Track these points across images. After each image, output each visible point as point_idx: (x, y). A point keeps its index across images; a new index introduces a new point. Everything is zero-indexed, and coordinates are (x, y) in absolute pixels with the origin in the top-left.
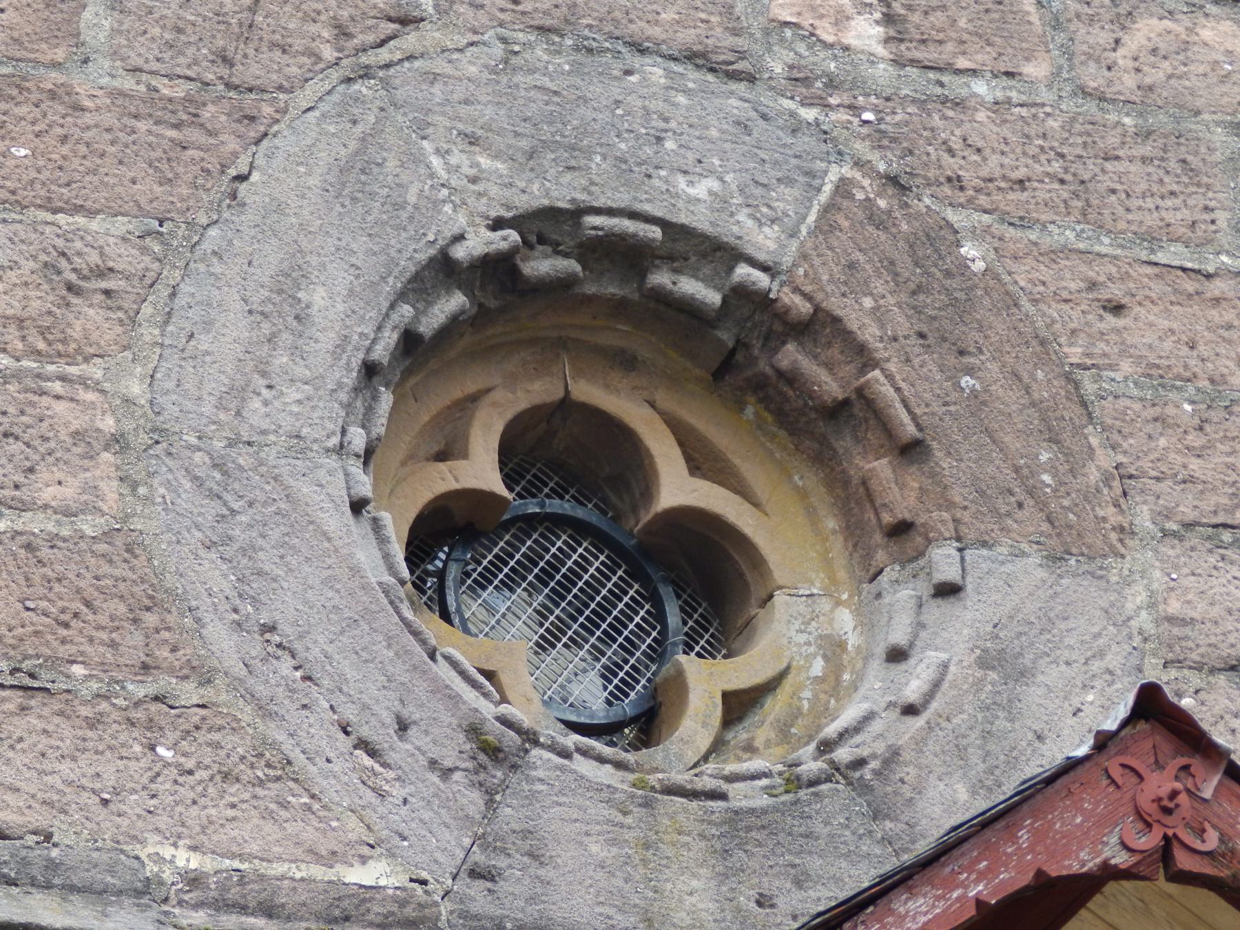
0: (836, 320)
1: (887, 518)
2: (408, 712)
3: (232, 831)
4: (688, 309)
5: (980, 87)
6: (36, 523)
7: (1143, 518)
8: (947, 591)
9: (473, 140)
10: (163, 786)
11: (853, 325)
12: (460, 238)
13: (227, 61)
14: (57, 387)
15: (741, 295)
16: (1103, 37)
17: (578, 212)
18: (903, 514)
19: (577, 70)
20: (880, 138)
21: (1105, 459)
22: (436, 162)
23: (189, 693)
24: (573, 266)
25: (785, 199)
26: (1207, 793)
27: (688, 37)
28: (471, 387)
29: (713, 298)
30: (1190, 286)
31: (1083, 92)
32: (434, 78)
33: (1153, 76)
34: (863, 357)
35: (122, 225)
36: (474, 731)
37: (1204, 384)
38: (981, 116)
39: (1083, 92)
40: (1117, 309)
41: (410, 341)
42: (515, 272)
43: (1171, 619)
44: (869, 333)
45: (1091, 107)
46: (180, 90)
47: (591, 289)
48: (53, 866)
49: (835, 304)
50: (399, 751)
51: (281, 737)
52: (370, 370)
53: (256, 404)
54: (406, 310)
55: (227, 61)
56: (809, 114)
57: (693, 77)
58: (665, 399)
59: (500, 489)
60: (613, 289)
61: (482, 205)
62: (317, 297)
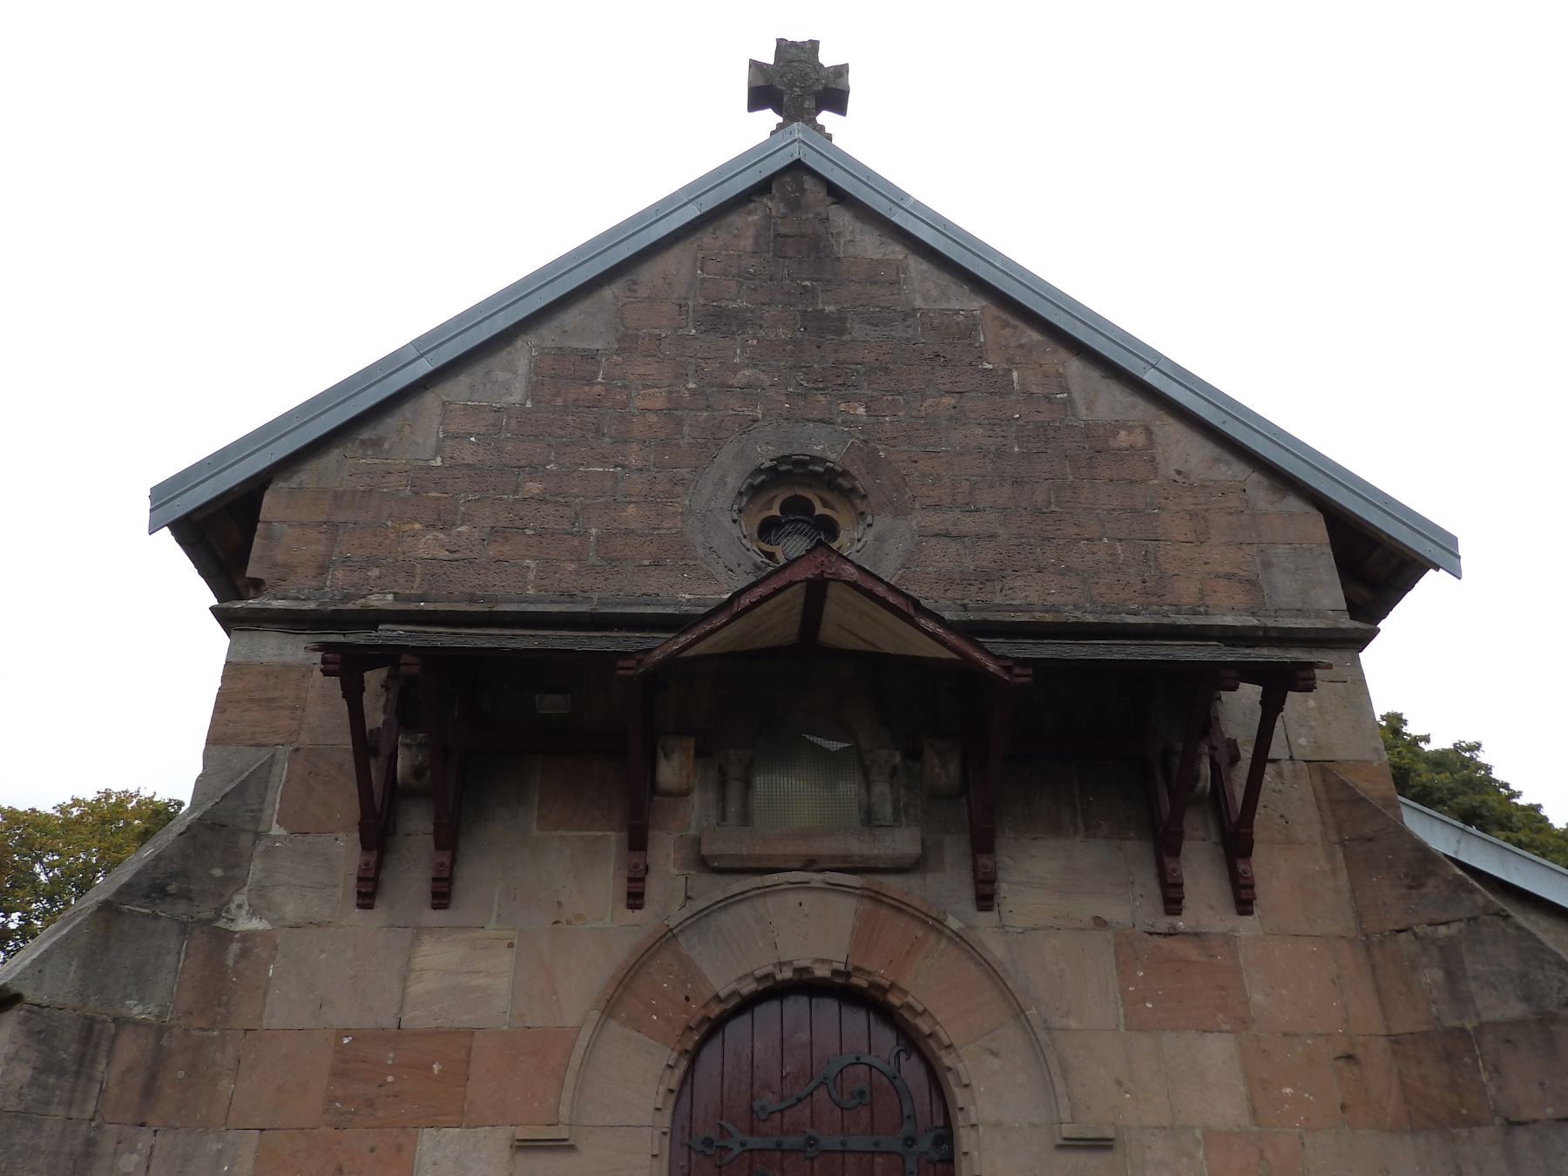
0: (848, 472)
1: (859, 511)
2: (740, 562)
3: (699, 590)
4: (817, 473)
5: (887, 419)
6: (663, 532)
7: (917, 506)
8: (870, 525)
9: (767, 443)
10: (684, 582)
11: (852, 472)
12: (763, 464)
13: (714, 434)
14: (670, 504)
15: (828, 470)
16: (918, 404)
17: (791, 456)
18: (862, 510)
19: (793, 426)
20: (862, 432)
21: (909, 494)
22: (759, 449)
23: (692, 563)
24: (791, 467)
25: (839, 448)
26: (833, 560)
27: (819, 417)
28: (773, 495)
29: (822, 470)
30: (934, 455)
31: (912, 417)
32: (759, 432)
33: (929, 411)
34: (854, 478)
35: (687, 470)
36: (755, 564)
37: (935, 476)
38: (887, 425)
39: (912, 417)
40: (916, 462)
41: (751, 486)
42: (777, 469)
43: (922, 527)
44: (856, 474)
45: (913, 420)
46: (703, 441)
47: (796, 471)
48: (658, 600)
49: (847, 468)
50: (738, 570)
51: (711, 569)
52: (740, 493)
53: (713, 503)
54: (749, 480)
55: (714, 434)
56: (846, 429)
57: (820, 425)
58: (818, 492)
59: (780, 515)
60: (801, 471)
61: (769, 457)
62: (729, 480)
